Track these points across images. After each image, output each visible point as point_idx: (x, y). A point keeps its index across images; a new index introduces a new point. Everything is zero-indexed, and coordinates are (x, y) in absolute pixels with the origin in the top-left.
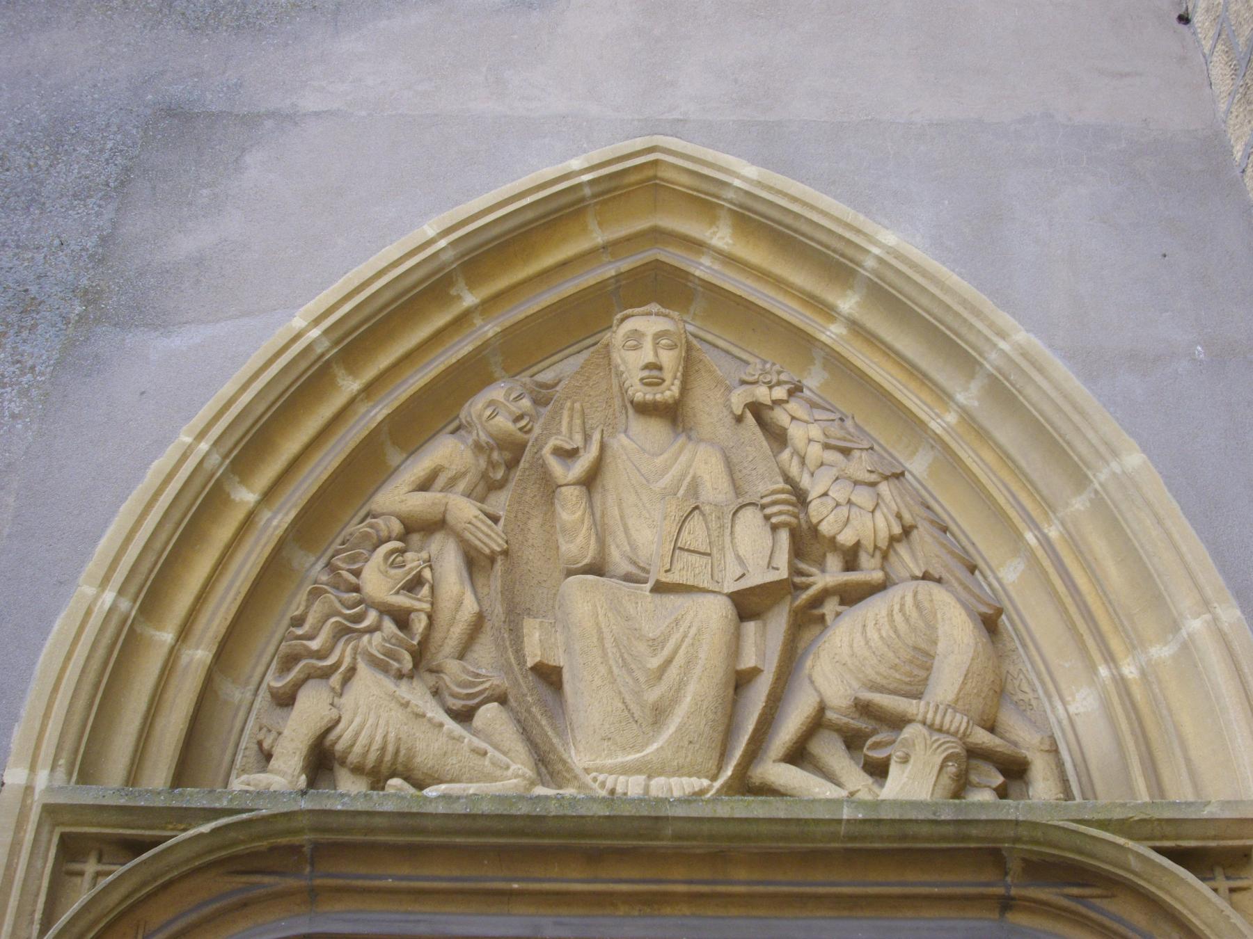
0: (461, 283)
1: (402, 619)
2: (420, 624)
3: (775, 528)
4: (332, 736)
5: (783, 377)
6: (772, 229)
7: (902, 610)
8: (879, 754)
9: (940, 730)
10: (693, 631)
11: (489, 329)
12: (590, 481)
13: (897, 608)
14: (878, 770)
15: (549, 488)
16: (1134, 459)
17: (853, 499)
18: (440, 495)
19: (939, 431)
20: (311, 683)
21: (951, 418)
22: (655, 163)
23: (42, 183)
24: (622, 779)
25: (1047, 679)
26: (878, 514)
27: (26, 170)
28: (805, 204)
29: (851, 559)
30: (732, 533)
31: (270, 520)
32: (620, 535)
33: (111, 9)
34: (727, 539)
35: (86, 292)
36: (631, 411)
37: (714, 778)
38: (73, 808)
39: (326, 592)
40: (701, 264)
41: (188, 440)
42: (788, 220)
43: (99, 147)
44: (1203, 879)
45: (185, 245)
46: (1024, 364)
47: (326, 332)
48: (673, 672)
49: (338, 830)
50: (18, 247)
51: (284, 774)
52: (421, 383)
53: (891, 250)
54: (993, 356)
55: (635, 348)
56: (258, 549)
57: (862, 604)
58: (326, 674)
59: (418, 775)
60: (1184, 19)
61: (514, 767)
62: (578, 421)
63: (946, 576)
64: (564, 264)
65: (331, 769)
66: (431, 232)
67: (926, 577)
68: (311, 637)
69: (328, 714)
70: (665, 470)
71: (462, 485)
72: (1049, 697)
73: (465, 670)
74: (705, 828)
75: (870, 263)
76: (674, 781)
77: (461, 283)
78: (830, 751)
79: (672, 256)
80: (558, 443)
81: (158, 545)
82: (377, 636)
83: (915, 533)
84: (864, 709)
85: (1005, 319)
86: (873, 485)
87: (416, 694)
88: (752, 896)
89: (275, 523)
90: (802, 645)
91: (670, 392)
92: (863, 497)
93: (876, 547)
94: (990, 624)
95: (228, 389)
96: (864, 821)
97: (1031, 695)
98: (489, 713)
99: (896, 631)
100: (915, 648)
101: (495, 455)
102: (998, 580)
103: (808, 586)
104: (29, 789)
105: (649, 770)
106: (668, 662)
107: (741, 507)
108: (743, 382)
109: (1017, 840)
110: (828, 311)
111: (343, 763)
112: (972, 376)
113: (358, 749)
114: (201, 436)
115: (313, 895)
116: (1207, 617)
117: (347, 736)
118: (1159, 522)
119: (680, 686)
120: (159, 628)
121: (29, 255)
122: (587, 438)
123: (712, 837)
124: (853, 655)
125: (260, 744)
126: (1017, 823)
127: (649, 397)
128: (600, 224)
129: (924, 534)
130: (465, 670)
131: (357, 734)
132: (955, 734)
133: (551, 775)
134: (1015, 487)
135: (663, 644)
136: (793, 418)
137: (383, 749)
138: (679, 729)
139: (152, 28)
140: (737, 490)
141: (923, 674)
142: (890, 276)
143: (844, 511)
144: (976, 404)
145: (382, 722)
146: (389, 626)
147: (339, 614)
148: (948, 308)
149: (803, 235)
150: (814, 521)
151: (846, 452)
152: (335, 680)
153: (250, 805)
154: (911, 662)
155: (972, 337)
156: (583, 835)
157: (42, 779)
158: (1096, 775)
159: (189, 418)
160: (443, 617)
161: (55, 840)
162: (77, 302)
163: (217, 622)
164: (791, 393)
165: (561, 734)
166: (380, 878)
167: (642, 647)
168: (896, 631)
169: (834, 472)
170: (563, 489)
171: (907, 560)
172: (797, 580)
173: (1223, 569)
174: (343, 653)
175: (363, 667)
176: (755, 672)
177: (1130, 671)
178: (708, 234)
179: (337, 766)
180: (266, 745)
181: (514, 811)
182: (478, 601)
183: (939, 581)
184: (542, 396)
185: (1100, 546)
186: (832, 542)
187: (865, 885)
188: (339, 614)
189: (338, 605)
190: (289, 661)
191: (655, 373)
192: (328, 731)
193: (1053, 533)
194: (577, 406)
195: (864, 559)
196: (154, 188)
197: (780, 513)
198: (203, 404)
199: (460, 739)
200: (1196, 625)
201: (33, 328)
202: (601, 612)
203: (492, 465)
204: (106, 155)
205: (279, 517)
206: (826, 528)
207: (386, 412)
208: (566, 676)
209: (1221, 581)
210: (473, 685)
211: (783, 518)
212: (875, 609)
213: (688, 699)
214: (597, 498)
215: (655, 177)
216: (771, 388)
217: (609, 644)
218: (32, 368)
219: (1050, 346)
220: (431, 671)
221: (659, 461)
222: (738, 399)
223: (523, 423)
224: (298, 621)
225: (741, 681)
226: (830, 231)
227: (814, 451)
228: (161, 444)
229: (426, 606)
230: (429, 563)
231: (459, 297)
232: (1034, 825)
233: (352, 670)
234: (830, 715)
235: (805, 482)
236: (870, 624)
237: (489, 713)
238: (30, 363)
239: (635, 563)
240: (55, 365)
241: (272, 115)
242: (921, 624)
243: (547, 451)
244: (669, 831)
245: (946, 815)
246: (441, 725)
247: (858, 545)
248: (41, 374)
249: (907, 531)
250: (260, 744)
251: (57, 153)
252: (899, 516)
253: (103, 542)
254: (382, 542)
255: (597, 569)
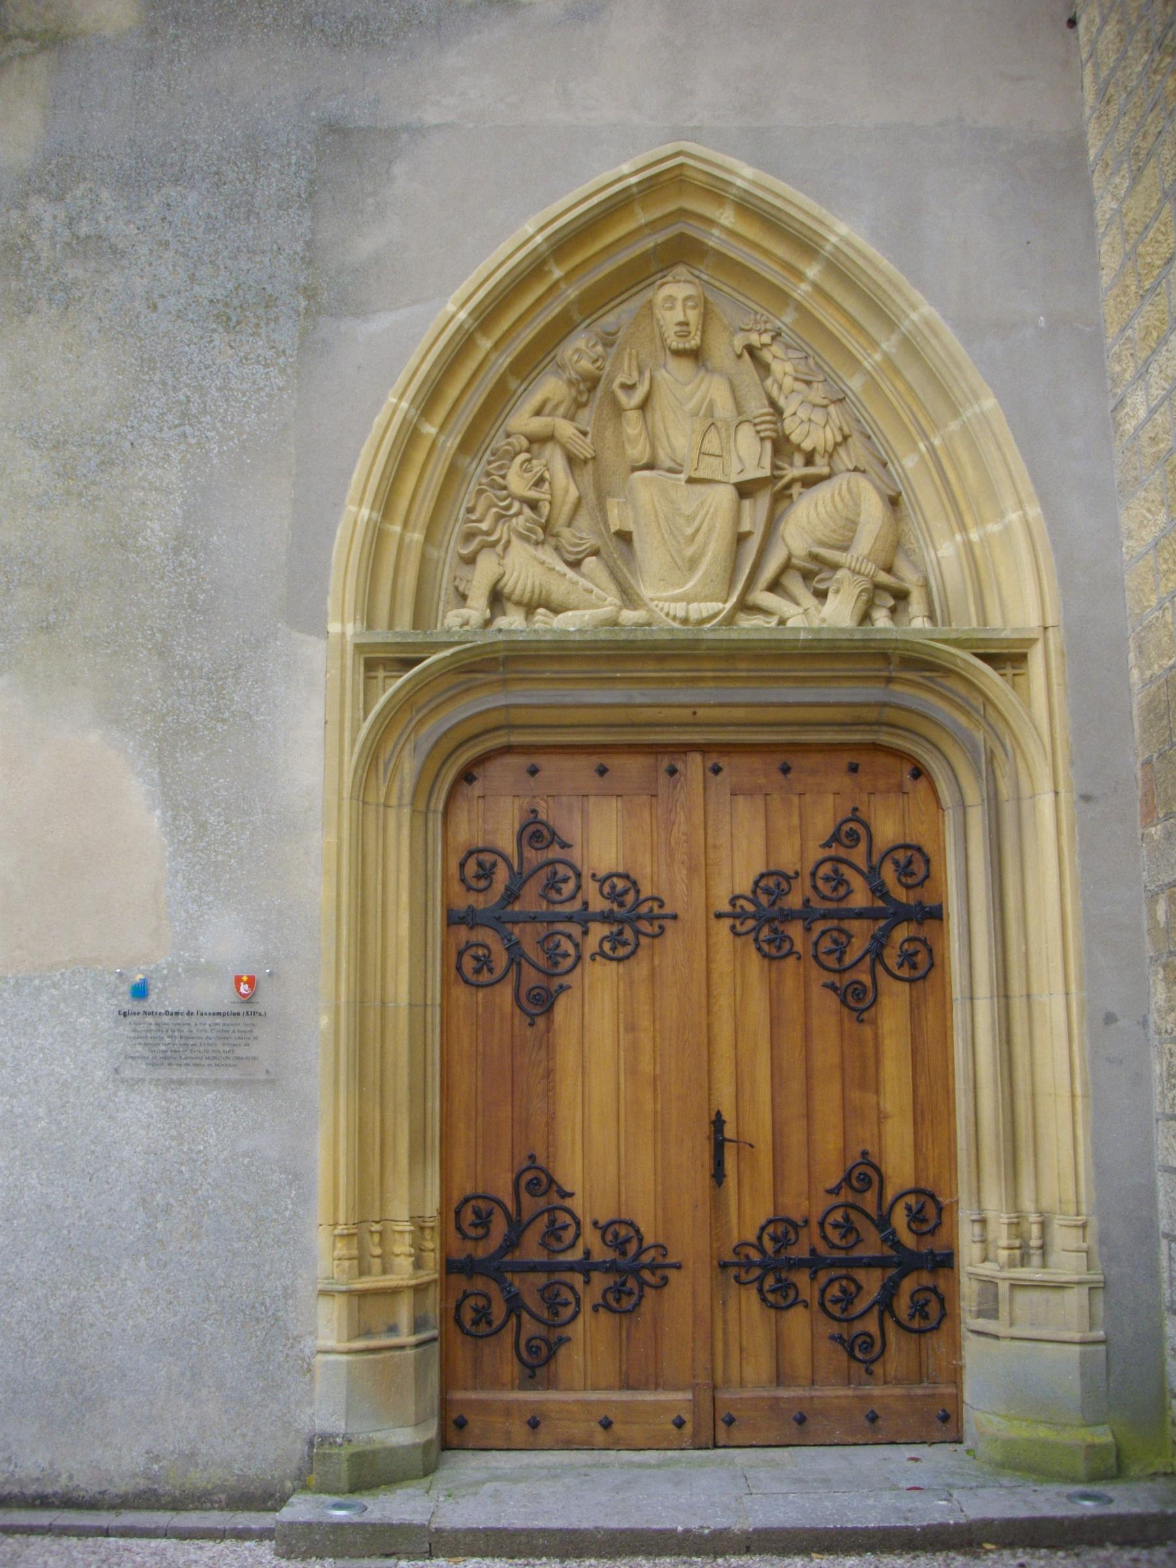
0: (551, 262)
1: (534, 505)
2: (545, 509)
3: (762, 439)
4: (502, 584)
5: (769, 326)
6: (762, 216)
7: (840, 494)
8: (822, 586)
9: (859, 573)
10: (712, 510)
11: (572, 293)
12: (643, 406)
13: (837, 492)
14: (822, 595)
15: (618, 410)
16: (989, 403)
17: (812, 418)
18: (549, 419)
19: (869, 368)
20: (485, 551)
21: (878, 357)
22: (681, 165)
23: (252, 196)
24: (672, 605)
25: (926, 534)
26: (828, 428)
27: (238, 184)
28: (785, 200)
29: (809, 460)
30: (735, 440)
31: (445, 442)
32: (665, 443)
33: (266, 26)
34: (732, 444)
35: (305, 289)
36: (668, 352)
37: (725, 602)
38: (370, 645)
39: (486, 491)
40: (712, 235)
41: (394, 400)
42: (774, 212)
43: (286, 162)
44: (995, 669)
45: (367, 245)
46: (926, 332)
47: (470, 314)
48: (700, 537)
49: (521, 650)
50: (249, 252)
51: (476, 609)
52: (530, 337)
53: (842, 239)
54: (907, 323)
55: (671, 308)
56: (441, 464)
57: (814, 488)
58: (493, 545)
59: (554, 605)
60: (1072, 23)
61: (610, 599)
62: (634, 363)
63: (868, 469)
64: (619, 240)
65: (501, 601)
66: (531, 230)
67: (856, 469)
68: (479, 521)
69: (498, 570)
70: (692, 396)
71: (561, 410)
72: (927, 545)
73: (574, 536)
74: (724, 645)
75: (828, 247)
76: (703, 605)
77: (551, 262)
78: (794, 584)
79: (692, 229)
80: (624, 380)
81: (387, 474)
82: (521, 519)
83: (850, 440)
84: (815, 557)
85: (916, 295)
86: (825, 406)
87: (547, 555)
88: (748, 678)
89: (449, 444)
90: (778, 512)
91: (694, 342)
92: (818, 416)
93: (825, 451)
94: (894, 502)
95: (413, 361)
96: (812, 640)
97: (915, 545)
98: (590, 563)
99: (835, 507)
100: (846, 519)
101: (582, 386)
102: (902, 467)
103: (782, 477)
104: (343, 634)
105: (688, 599)
106: (698, 530)
107: (740, 423)
108: (743, 330)
109: (897, 648)
110: (800, 276)
111: (509, 599)
112: (893, 331)
113: (517, 592)
114: (401, 397)
115: (504, 682)
116: (1021, 513)
117: (511, 584)
118: (999, 447)
119: (705, 545)
120: (392, 523)
121: (258, 259)
122: (641, 373)
123: (727, 649)
124: (809, 522)
125: (457, 588)
126: (896, 640)
127: (681, 346)
128: (643, 208)
129: (856, 441)
130: (574, 536)
131: (516, 583)
132: (867, 576)
133: (630, 601)
134: (915, 409)
135: (694, 519)
136: (775, 357)
137: (533, 592)
138: (705, 573)
139: (301, 46)
140: (740, 413)
141: (850, 534)
142: (842, 258)
143: (806, 426)
144: (894, 350)
145: (530, 574)
146: (527, 511)
147: (497, 506)
148: (879, 286)
149: (784, 223)
150: (787, 432)
151: (808, 383)
152: (499, 548)
153: (470, 638)
154: (844, 527)
155: (893, 308)
156: (657, 649)
157: (350, 629)
158: (950, 596)
159: (392, 385)
160: (558, 500)
161: (362, 662)
162: (301, 298)
163: (423, 515)
164: (773, 338)
165: (633, 574)
166: (542, 672)
167: (681, 521)
168: (835, 507)
169: (800, 398)
170: (628, 413)
171: (845, 459)
172: (777, 473)
173: (1034, 480)
174: (501, 532)
175: (515, 541)
176: (749, 534)
177: (974, 536)
178: (717, 214)
179: (504, 601)
180: (461, 589)
181: (618, 638)
182: (578, 489)
183: (864, 472)
184: (608, 340)
185: (964, 456)
186: (798, 447)
187: (811, 671)
188: (497, 506)
189: (495, 500)
190: (469, 536)
191: (684, 328)
192: (499, 581)
193: (937, 442)
194: (634, 352)
195: (818, 459)
196: (334, 199)
197: (766, 430)
198: (399, 373)
199: (576, 583)
200: (1013, 517)
201: (276, 319)
202: (656, 499)
203: (580, 392)
204: (293, 169)
205: (451, 440)
206: (794, 438)
207: (509, 360)
208: (635, 538)
209: (1032, 489)
210: (580, 545)
211: (768, 433)
212: (823, 492)
213: (710, 554)
214: (649, 415)
215: (681, 175)
216: (760, 334)
217: (662, 521)
218: (284, 352)
219: (944, 317)
220: (553, 536)
221: (688, 389)
222: (739, 342)
223: (598, 364)
224: (470, 510)
225: (741, 539)
226: (802, 223)
227: (788, 382)
228: (378, 404)
229: (548, 497)
230: (547, 467)
231: (550, 272)
232: (906, 641)
233: (508, 542)
234: (795, 561)
235: (782, 402)
236: (820, 503)
237: (590, 563)
238: (281, 348)
239: (674, 461)
240: (299, 349)
241: (407, 128)
242: (851, 503)
243: (616, 385)
244: (704, 646)
245: (858, 636)
246: (565, 575)
247: (814, 450)
248: (291, 356)
249: (845, 438)
250: (457, 588)
251: (257, 168)
252: (841, 429)
253: (355, 476)
254: (517, 454)
255: (650, 466)
